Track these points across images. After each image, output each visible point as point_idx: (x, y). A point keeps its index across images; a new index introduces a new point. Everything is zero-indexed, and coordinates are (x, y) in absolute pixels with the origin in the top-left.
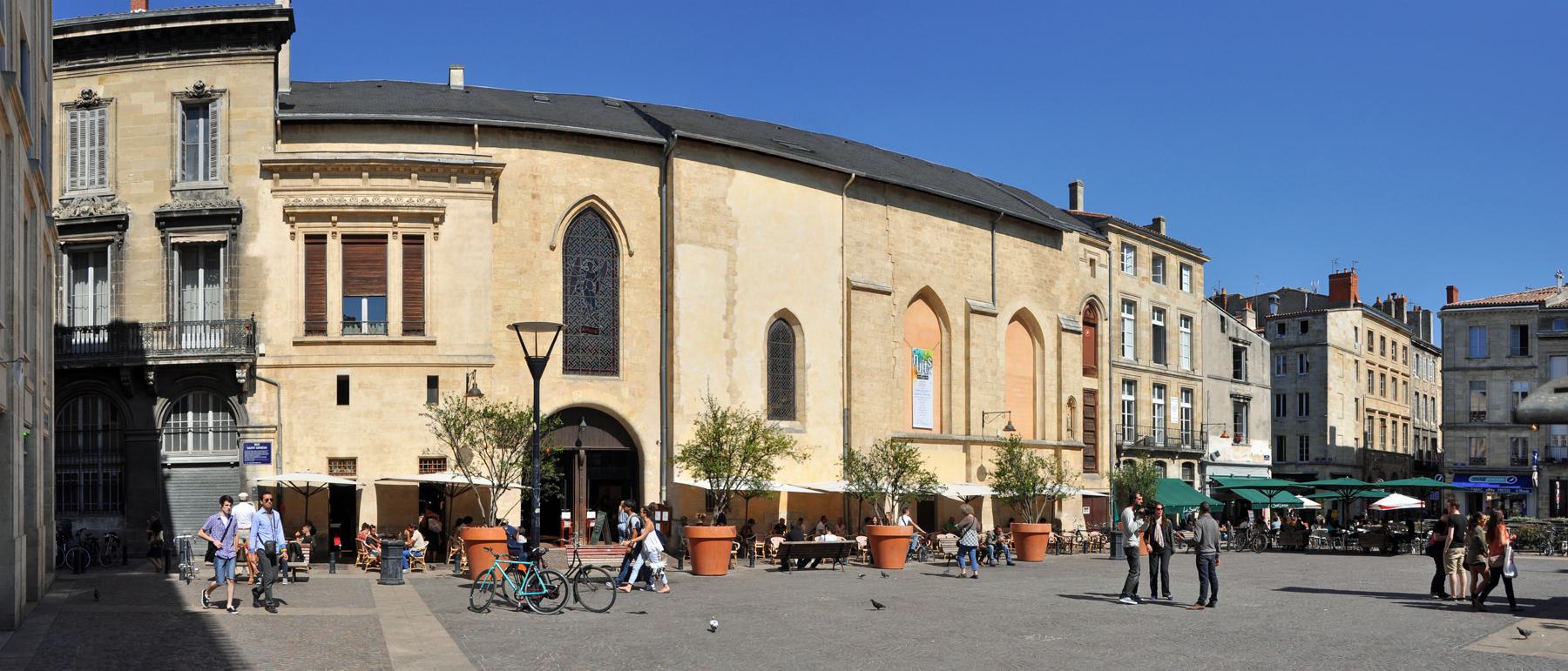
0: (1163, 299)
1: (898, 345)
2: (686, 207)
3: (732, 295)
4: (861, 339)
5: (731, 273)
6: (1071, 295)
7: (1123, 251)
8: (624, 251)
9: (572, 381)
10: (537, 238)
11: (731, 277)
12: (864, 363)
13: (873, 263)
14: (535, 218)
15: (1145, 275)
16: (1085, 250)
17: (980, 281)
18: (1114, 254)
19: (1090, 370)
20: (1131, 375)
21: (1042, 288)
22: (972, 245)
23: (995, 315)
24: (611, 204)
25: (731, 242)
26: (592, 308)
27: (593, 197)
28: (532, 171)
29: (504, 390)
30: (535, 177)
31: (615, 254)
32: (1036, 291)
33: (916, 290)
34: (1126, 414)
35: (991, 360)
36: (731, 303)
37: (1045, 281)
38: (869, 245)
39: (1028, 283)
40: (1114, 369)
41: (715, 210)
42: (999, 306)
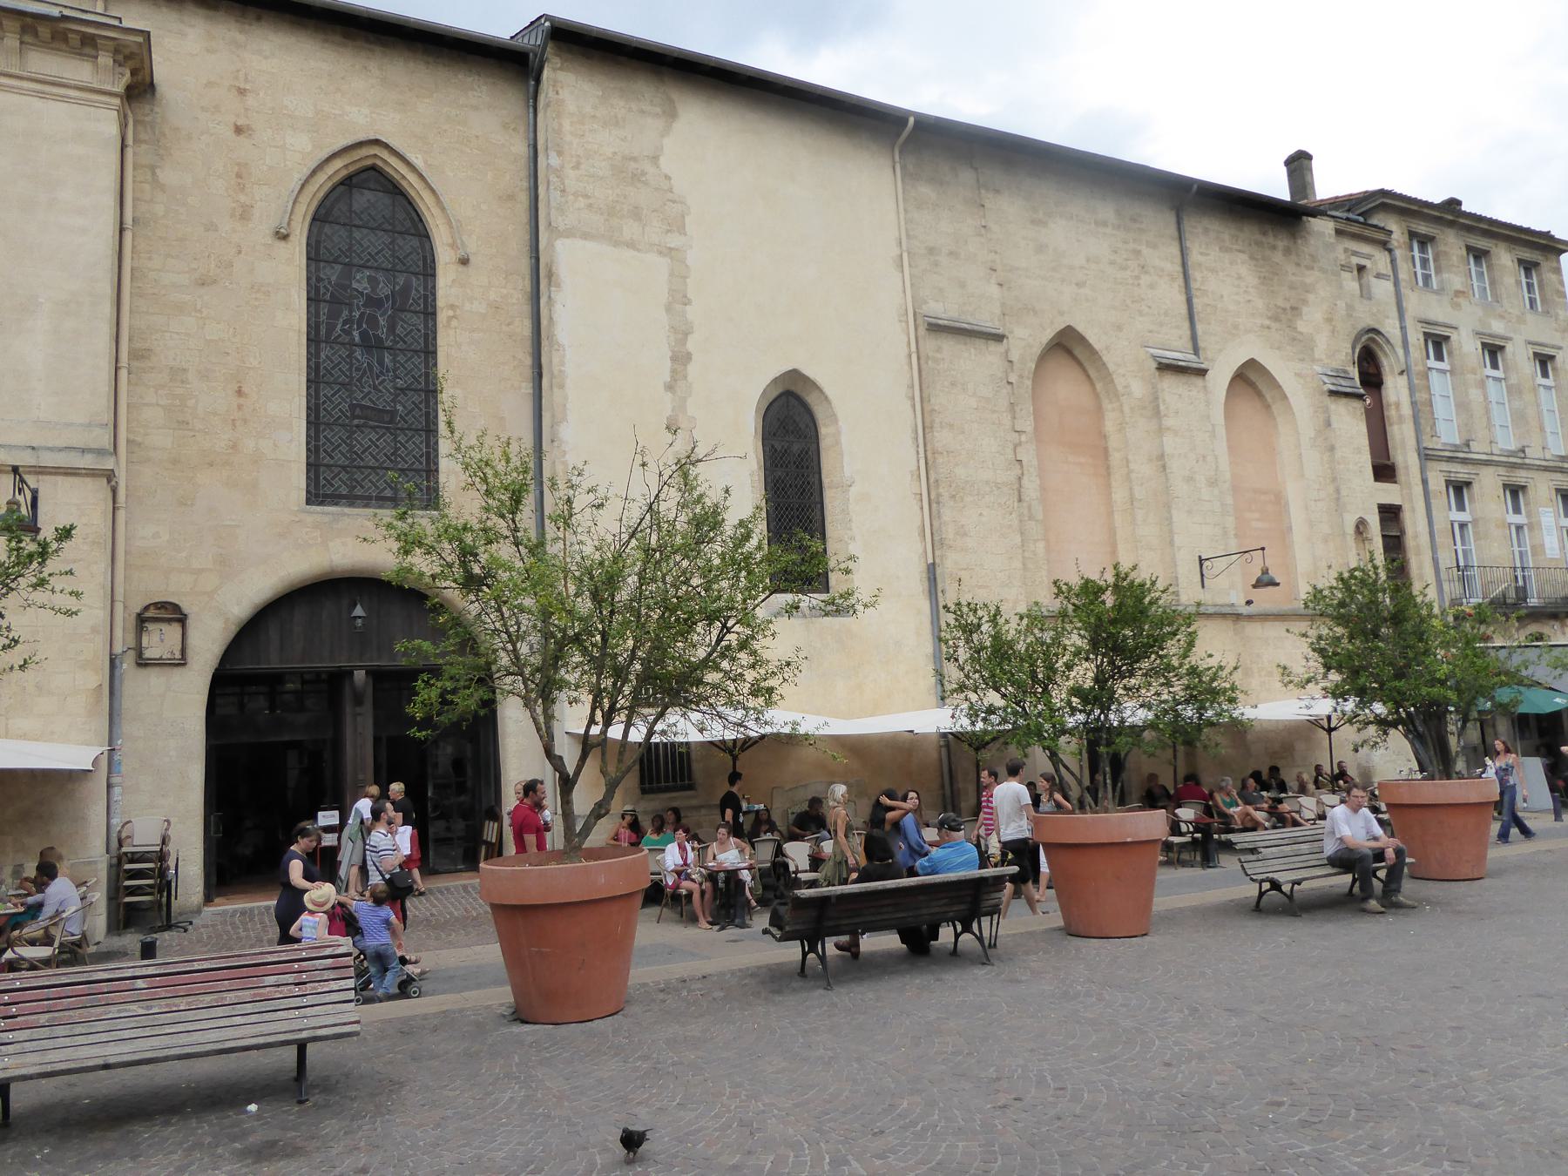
0: (1498, 327)
1: (1023, 438)
2: (577, 166)
3: (683, 341)
4: (951, 426)
5: (678, 299)
6: (1333, 332)
7: (1412, 249)
8: (444, 256)
9: (326, 519)
10: (244, 214)
11: (678, 307)
12: (961, 472)
13: (963, 285)
14: (241, 176)
15: (1459, 287)
16: (1346, 250)
17: (1166, 314)
18: (1398, 253)
19: (1384, 471)
20: (1461, 472)
21: (1280, 321)
22: (1145, 251)
23: (1202, 372)
24: (418, 162)
25: (674, 241)
26: (376, 369)
27: (377, 142)
28: (236, 78)
29: (156, 535)
30: (242, 92)
31: (428, 270)
32: (1269, 328)
33: (1048, 335)
34: (1459, 547)
35: (1204, 457)
36: (681, 359)
37: (1284, 309)
38: (951, 253)
39: (1253, 314)
40: (1430, 464)
41: (637, 178)
42: (1206, 359)
